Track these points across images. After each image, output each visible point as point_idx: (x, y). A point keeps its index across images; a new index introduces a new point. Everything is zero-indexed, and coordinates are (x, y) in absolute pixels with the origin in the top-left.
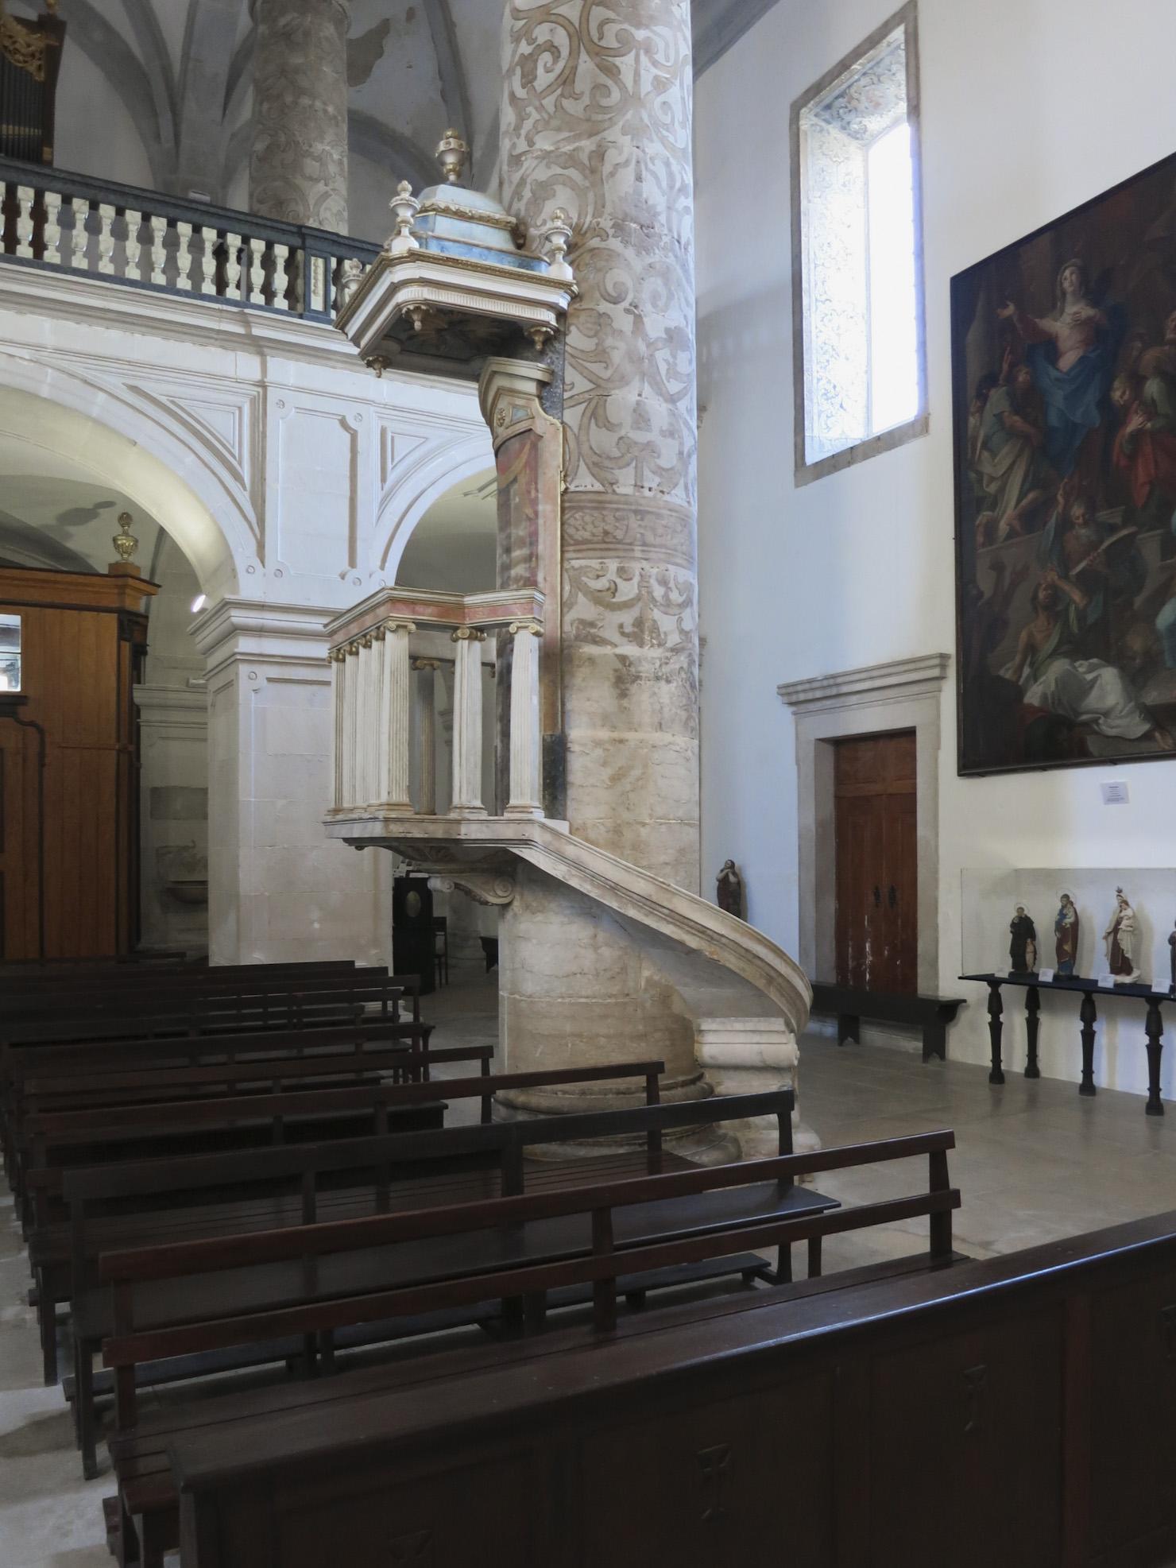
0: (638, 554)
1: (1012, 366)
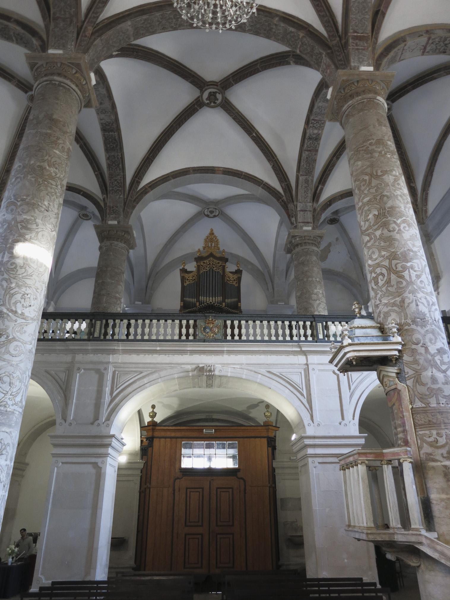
0: (443, 427)
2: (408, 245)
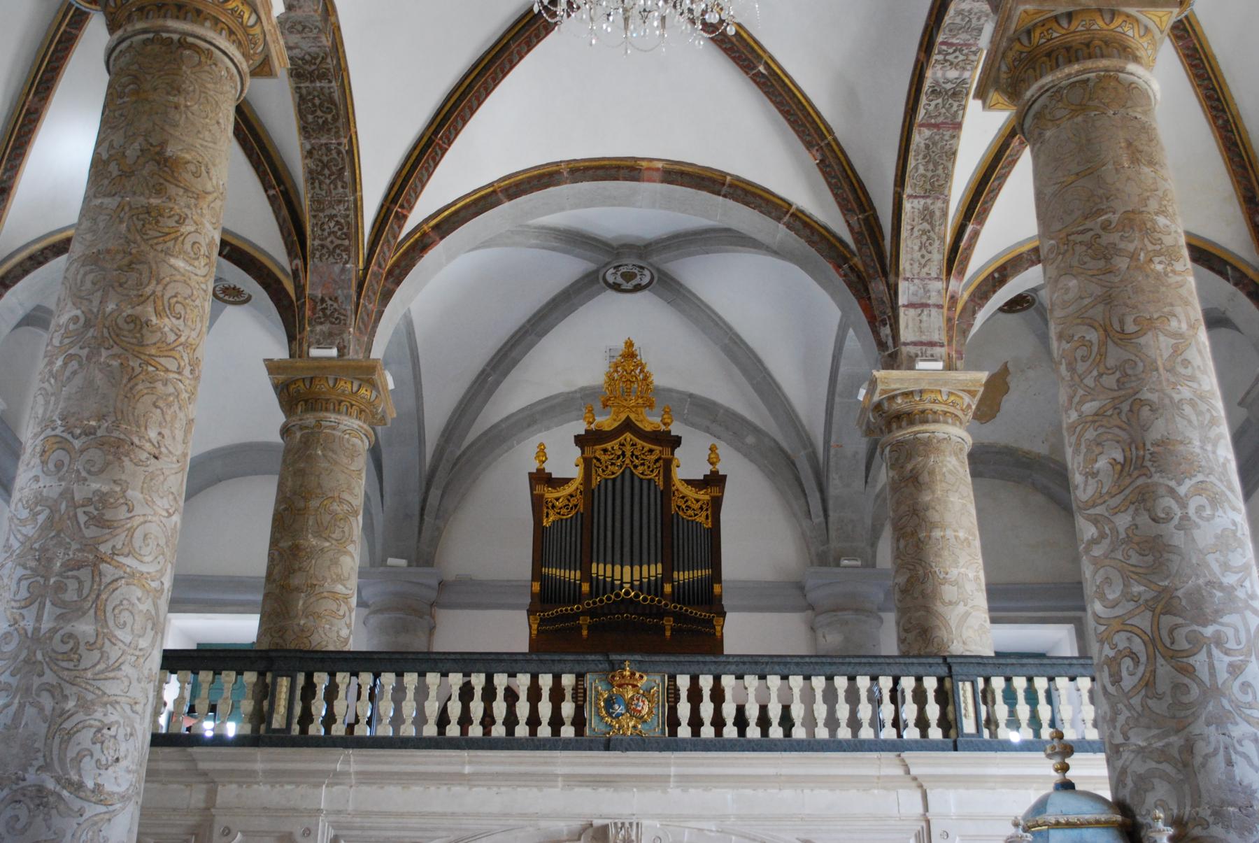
2: (1208, 566)
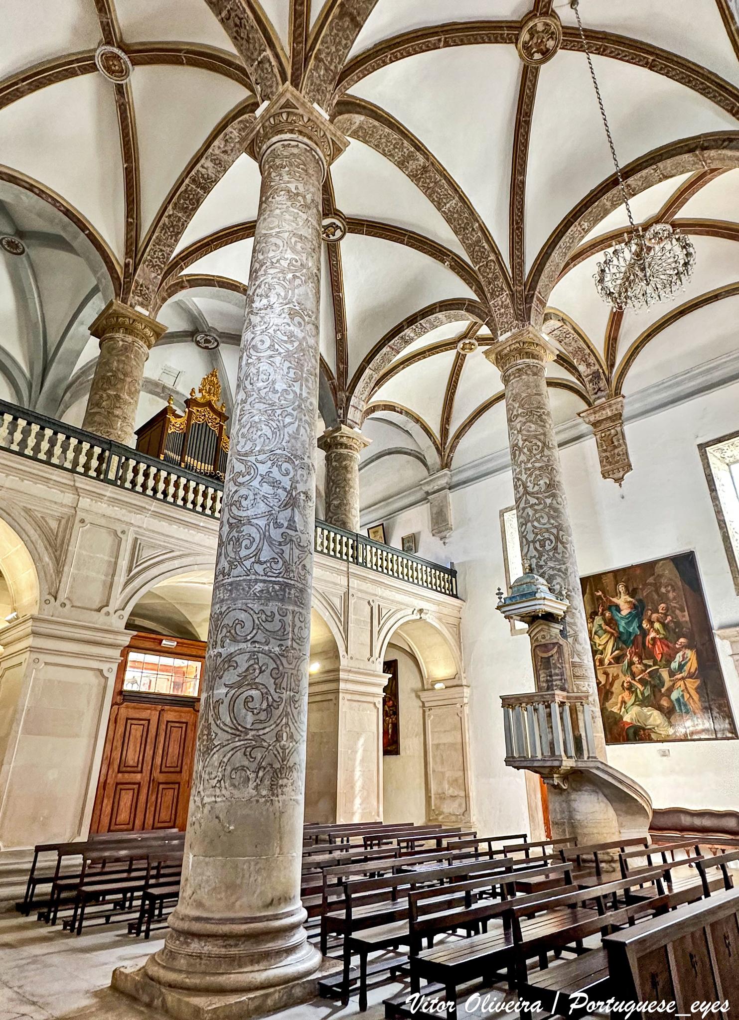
1: (603, 610)
